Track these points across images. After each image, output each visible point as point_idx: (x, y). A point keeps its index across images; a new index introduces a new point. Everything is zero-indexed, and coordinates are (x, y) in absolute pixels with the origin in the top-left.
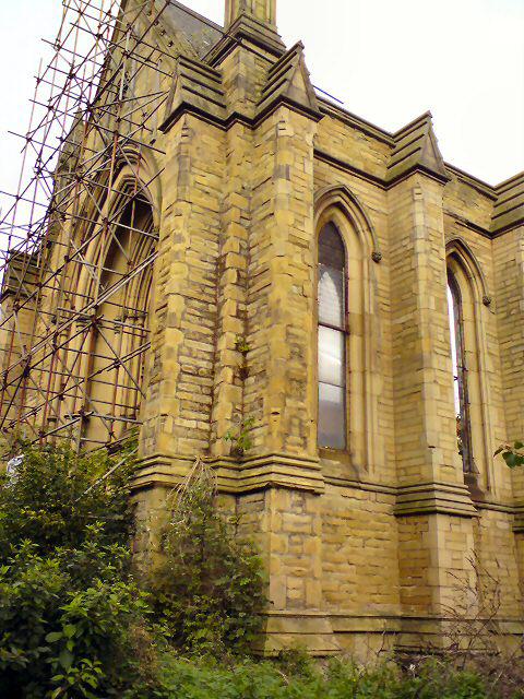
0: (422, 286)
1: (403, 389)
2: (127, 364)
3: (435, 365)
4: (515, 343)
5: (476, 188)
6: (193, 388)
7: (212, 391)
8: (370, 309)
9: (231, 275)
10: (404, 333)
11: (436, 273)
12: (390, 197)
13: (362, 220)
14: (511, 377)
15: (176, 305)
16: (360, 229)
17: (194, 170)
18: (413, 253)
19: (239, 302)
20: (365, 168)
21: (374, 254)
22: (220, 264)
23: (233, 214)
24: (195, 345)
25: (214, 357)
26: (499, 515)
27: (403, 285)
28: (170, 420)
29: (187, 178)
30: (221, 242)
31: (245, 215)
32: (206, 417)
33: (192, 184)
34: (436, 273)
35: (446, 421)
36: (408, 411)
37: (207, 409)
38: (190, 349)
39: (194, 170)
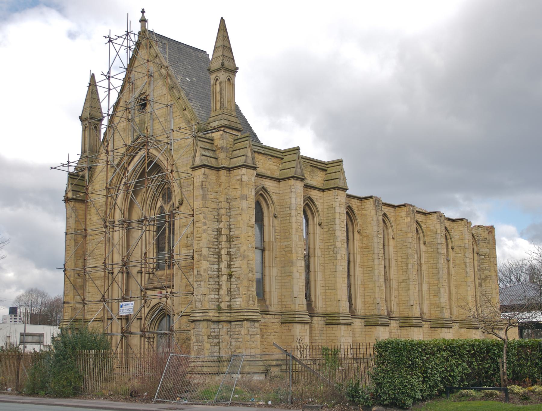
0: (294, 230)
1: (285, 273)
2: (117, 246)
3: (298, 265)
4: (330, 244)
5: (317, 168)
6: (213, 283)
7: (219, 283)
8: (273, 239)
9: (224, 238)
10: (286, 249)
11: (299, 224)
12: (281, 186)
13: (270, 200)
14: (328, 259)
15: (205, 251)
16: (269, 203)
17: (209, 193)
18: (290, 215)
19: (228, 248)
20: (271, 173)
21: (274, 214)
22: (219, 231)
23: (223, 211)
24: (212, 266)
25: (219, 270)
26: (320, 318)
27: (286, 228)
28: (207, 296)
29: (206, 198)
30: (219, 221)
31: (228, 211)
32: (217, 293)
33: (208, 199)
34: (299, 224)
35: (301, 287)
36: (287, 282)
37: (218, 290)
38: (211, 268)
39: (209, 193)
